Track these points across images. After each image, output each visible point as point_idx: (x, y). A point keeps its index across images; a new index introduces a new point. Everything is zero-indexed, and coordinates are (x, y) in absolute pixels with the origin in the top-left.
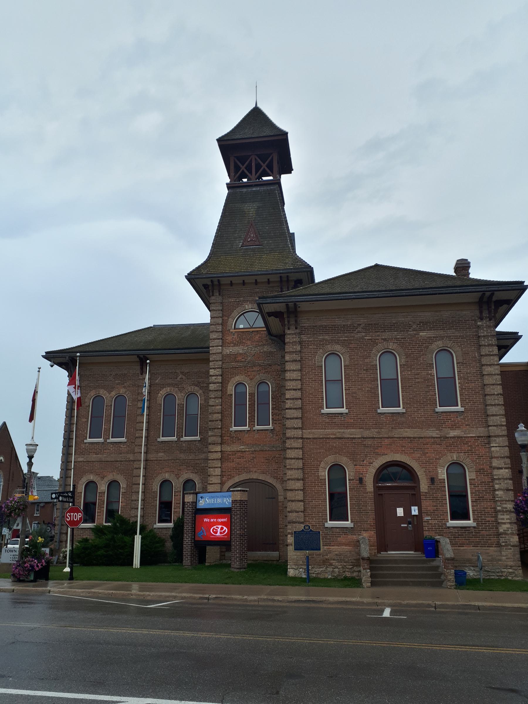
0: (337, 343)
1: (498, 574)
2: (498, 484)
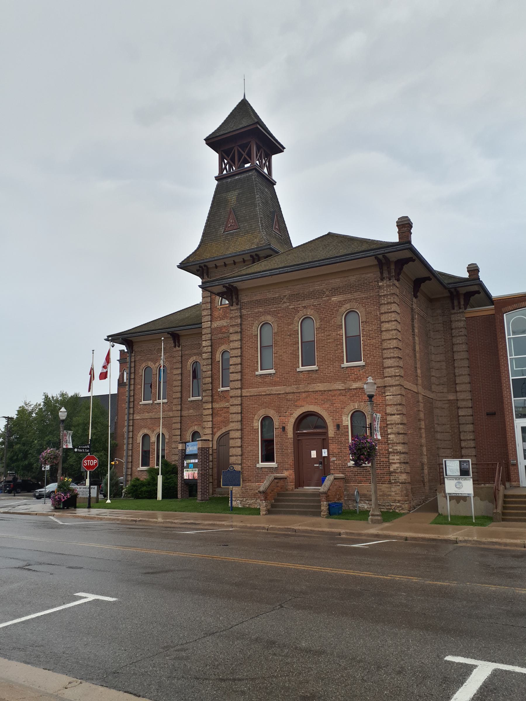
0: (269, 314)
1: (387, 508)
2: (390, 428)
